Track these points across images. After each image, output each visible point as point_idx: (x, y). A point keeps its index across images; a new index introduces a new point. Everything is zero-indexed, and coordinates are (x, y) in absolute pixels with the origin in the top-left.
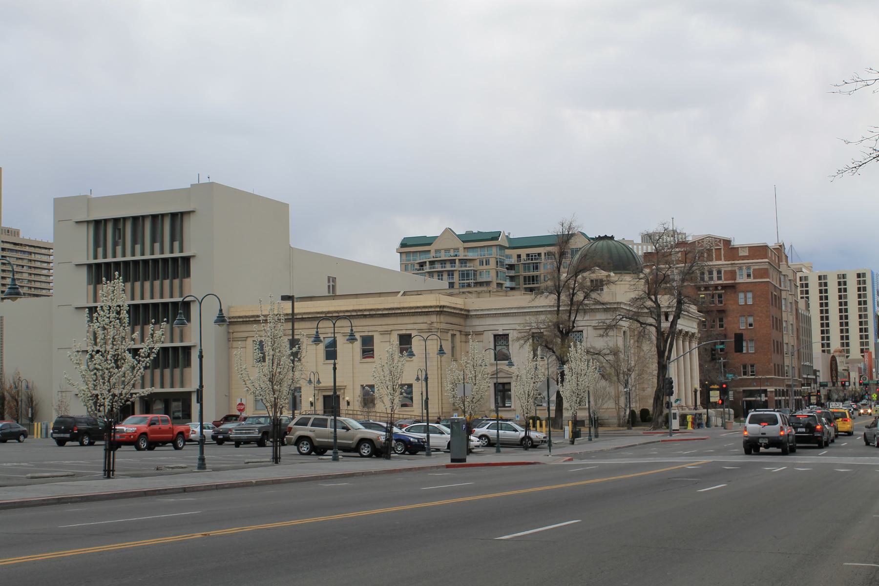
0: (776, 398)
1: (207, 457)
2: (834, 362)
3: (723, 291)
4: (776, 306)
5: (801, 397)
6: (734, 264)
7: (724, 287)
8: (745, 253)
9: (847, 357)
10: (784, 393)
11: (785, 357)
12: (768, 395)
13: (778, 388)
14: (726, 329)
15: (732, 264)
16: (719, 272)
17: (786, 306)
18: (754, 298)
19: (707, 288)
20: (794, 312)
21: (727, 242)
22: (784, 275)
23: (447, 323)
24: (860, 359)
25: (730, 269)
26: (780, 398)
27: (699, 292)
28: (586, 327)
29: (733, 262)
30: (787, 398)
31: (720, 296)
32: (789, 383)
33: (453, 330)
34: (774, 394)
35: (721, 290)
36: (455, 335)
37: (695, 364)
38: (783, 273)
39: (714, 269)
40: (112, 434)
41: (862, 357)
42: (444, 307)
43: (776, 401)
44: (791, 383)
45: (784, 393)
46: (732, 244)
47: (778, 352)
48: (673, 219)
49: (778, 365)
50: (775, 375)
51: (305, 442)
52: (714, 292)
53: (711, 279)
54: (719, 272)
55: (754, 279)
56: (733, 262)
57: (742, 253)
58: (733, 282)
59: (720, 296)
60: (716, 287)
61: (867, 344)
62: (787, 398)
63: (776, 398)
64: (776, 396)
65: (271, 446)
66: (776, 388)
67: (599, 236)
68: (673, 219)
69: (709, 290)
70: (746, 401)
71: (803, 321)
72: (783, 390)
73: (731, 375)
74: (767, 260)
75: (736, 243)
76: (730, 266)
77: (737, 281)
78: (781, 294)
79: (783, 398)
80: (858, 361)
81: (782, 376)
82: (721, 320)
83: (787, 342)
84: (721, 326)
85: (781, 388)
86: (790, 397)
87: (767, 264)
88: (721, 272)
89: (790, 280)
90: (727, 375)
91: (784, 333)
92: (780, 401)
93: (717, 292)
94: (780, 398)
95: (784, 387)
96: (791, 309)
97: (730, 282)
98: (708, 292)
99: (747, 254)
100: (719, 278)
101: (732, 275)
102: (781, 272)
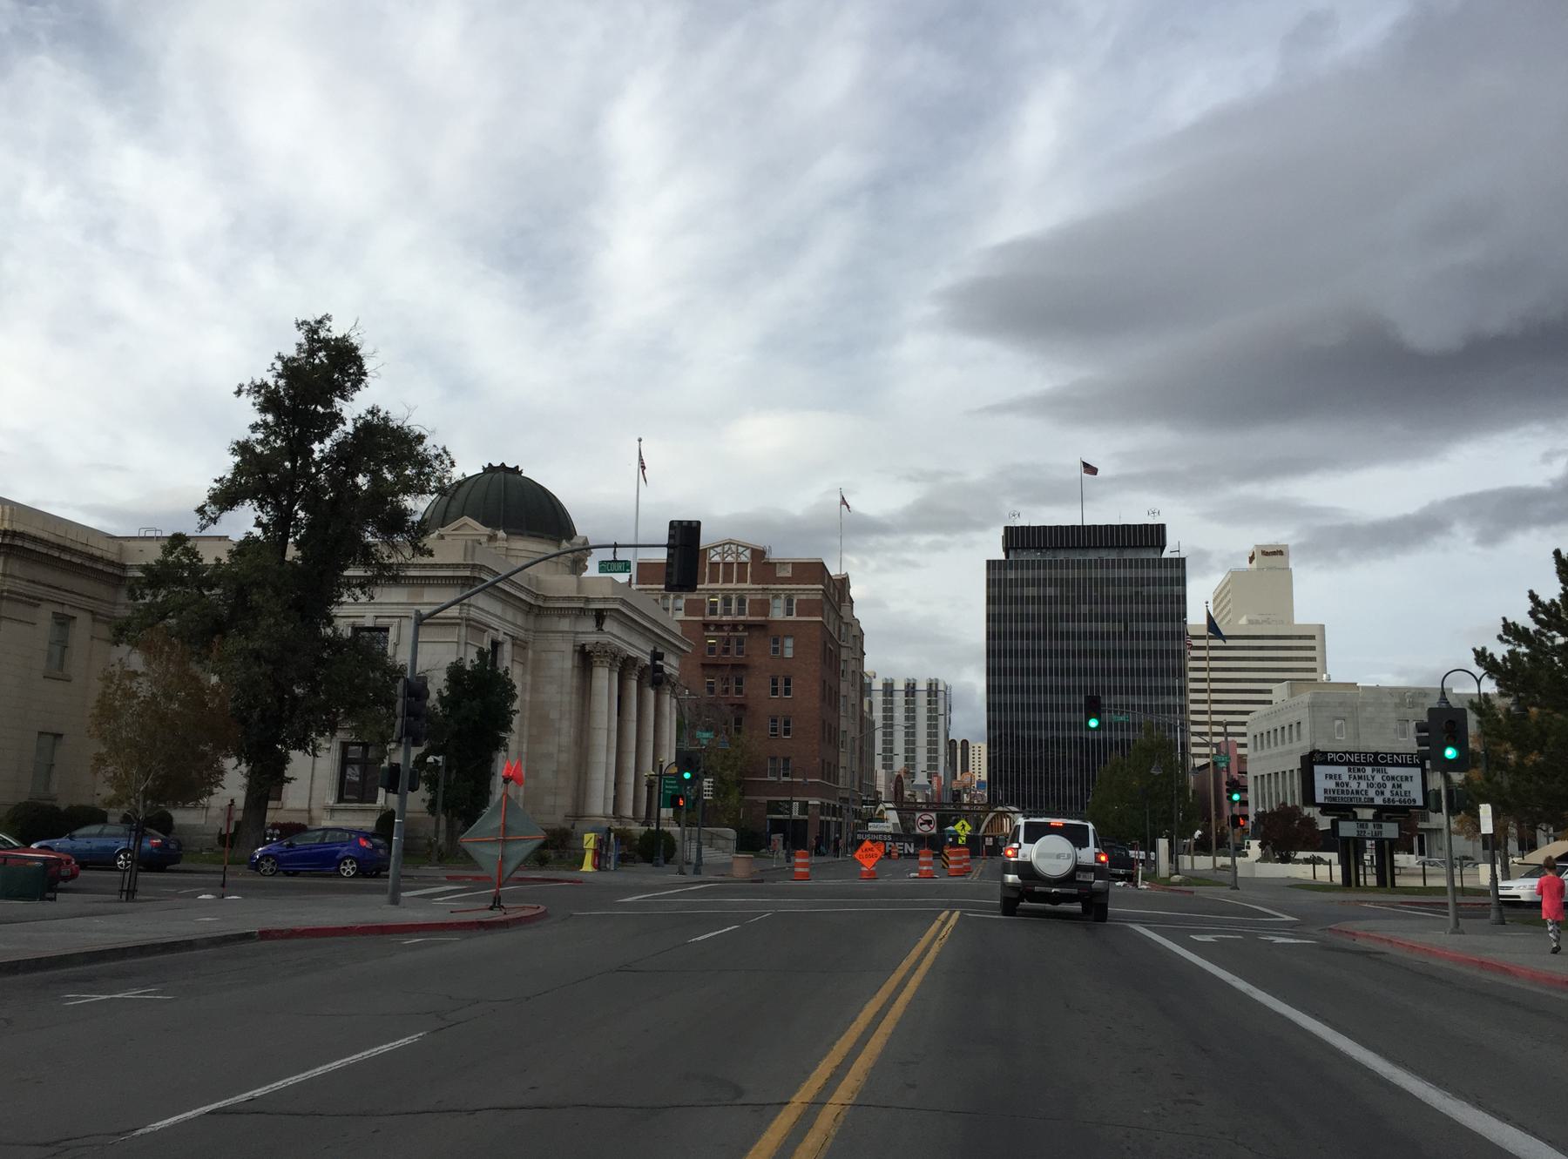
0: (822, 818)
1: (231, 879)
2: (900, 784)
3: (746, 634)
4: (830, 687)
5: (860, 822)
6: (767, 589)
7: (749, 626)
8: (787, 573)
9: (913, 781)
10: (835, 811)
11: (841, 754)
12: (810, 812)
13: (826, 801)
14: (746, 695)
15: (764, 589)
16: (741, 602)
17: (846, 711)
18: (795, 647)
19: (719, 626)
20: (858, 719)
21: (758, 554)
22: (847, 623)
23: (28, 581)
24: (927, 785)
25: (759, 597)
26: (829, 818)
27: (706, 634)
28: (397, 620)
29: (765, 586)
30: (840, 819)
31: (740, 642)
32: (843, 796)
33: (63, 604)
34: (818, 810)
35: (743, 631)
36: (74, 618)
37: (668, 734)
38: (845, 621)
39: (734, 597)
40: (1121, 872)
41: (928, 783)
42: (22, 535)
43: (822, 822)
44: (847, 796)
45: (835, 811)
46: (766, 557)
47: (830, 742)
48: (640, 440)
49: (829, 764)
50: (823, 779)
51: (348, 861)
52: (731, 634)
53: (727, 612)
54: (741, 602)
55: (798, 616)
56: (765, 586)
57: (781, 574)
58: (764, 618)
59: (740, 642)
60: (734, 626)
61: (936, 767)
62: (840, 819)
63: (822, 818)
64: (822, 814)
65: (1314, 867)
66: (824, 800)
67: (490, 464)
68: (640, 440)
69: (723, 631)
70: (771, 820)
71: (866, 725)
72: (834, 806)
73: (707, 735)
74: (821, 587)
75: (774, 556)
76: (761, 592)
77: (769, 618)
78: (840, 652)
79: (834, 819)
80: (924, 787)
81: (834, 783)
82: (739, 682)
83: (845, 694)
84: (739, 691)
85: (832, 802)
86: (844, 818)
87: (821, 592)
88: (745, 601)
89: (854, 636)
90: (699, 734)
91: (842, 714)
92: (828, 822)
93: (736, 634)
94: (829, 818)
95: (835, 800)
96: (854, 713)
97: (759, 618)
98: (721, 634)
99: (789, 575)
100: (741, 612)
101: (764, 607)
102: (841, 617)
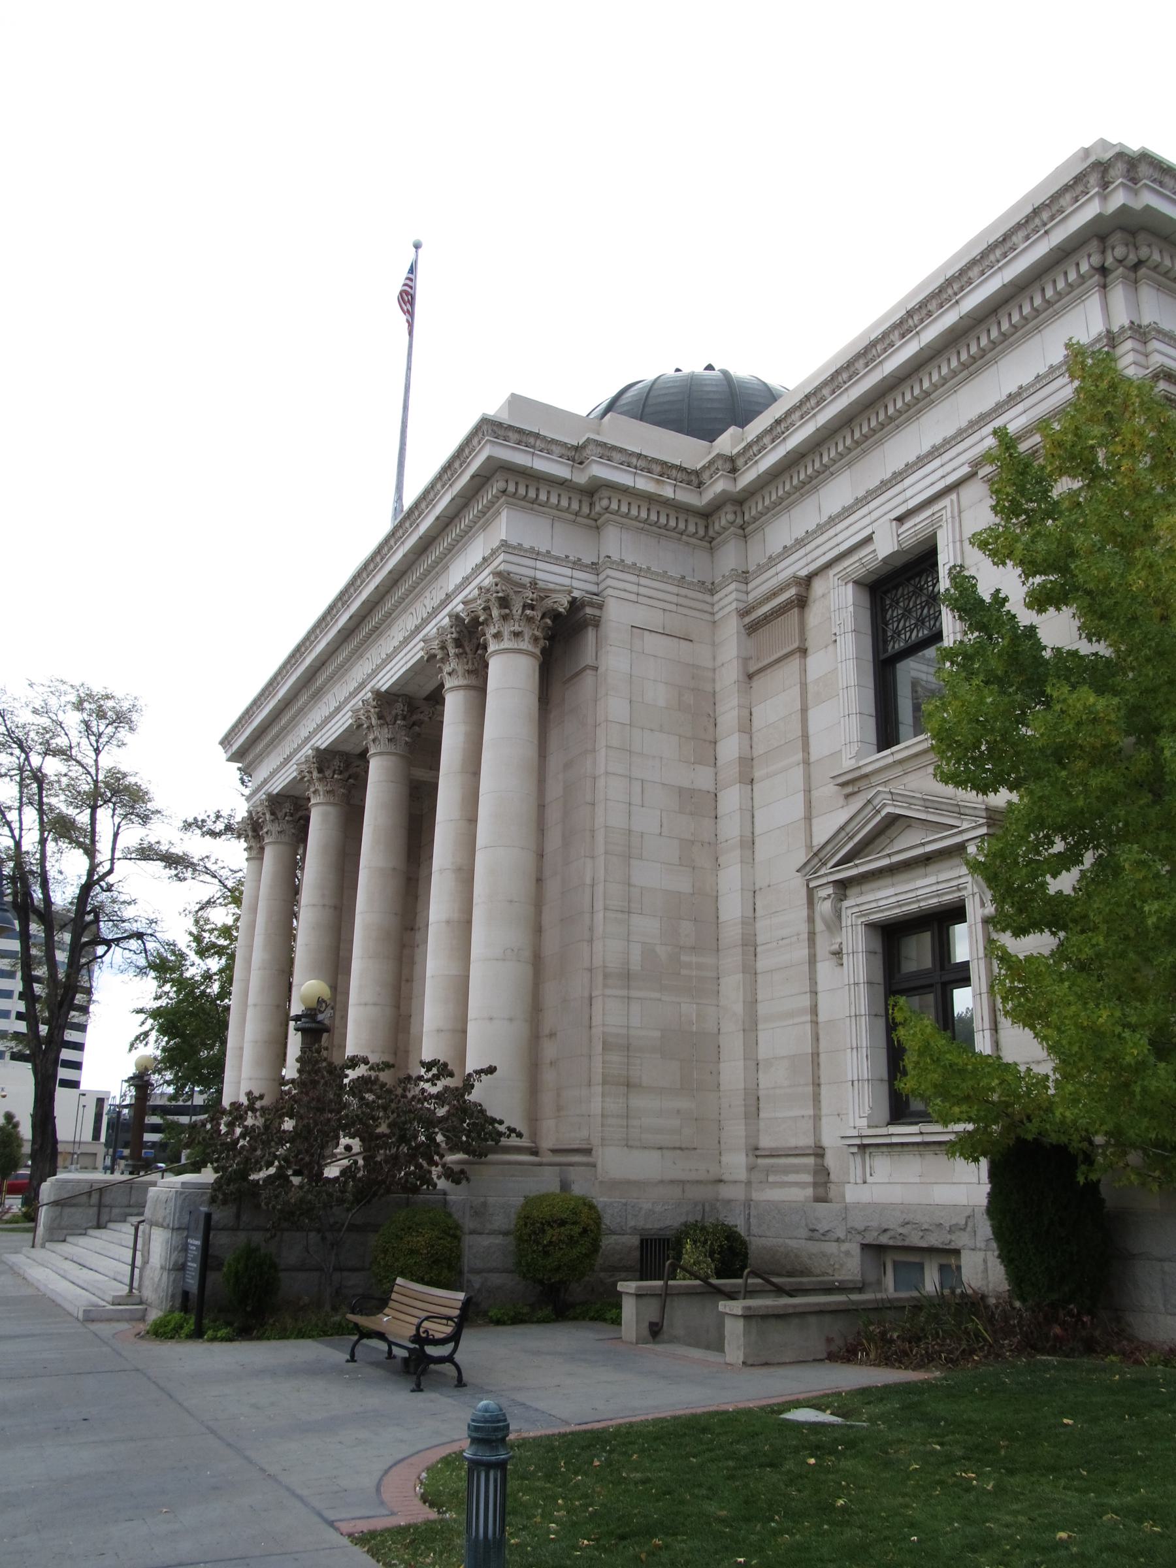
48: (417, 246)
68: (417, 246)
